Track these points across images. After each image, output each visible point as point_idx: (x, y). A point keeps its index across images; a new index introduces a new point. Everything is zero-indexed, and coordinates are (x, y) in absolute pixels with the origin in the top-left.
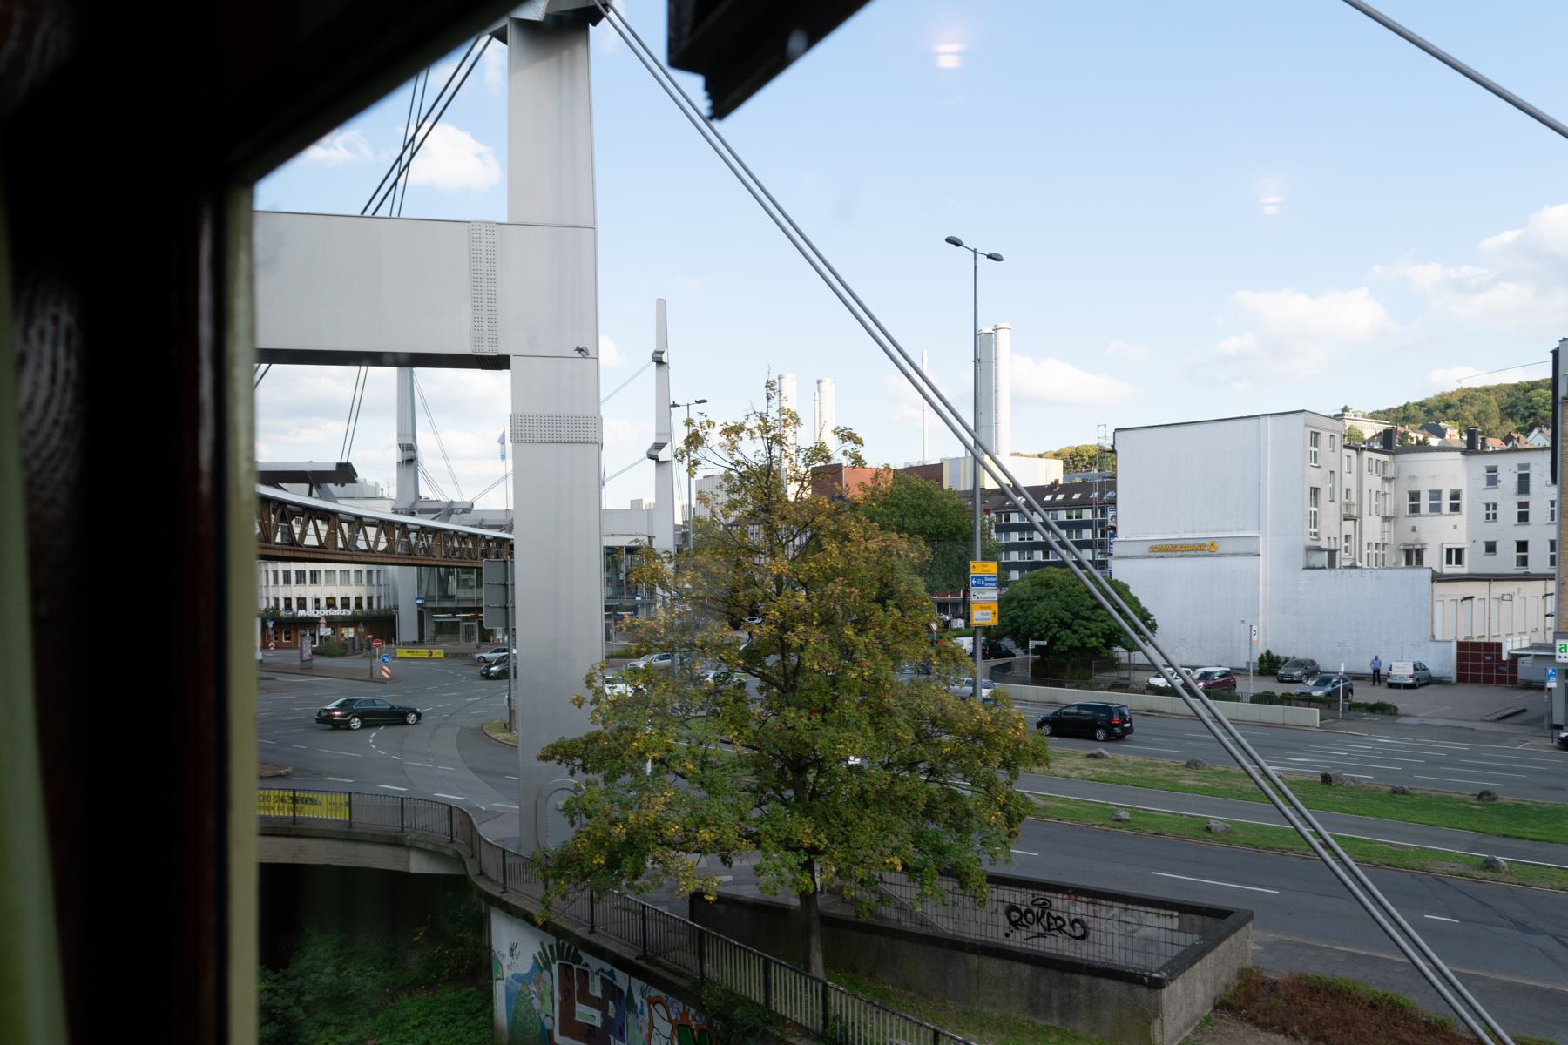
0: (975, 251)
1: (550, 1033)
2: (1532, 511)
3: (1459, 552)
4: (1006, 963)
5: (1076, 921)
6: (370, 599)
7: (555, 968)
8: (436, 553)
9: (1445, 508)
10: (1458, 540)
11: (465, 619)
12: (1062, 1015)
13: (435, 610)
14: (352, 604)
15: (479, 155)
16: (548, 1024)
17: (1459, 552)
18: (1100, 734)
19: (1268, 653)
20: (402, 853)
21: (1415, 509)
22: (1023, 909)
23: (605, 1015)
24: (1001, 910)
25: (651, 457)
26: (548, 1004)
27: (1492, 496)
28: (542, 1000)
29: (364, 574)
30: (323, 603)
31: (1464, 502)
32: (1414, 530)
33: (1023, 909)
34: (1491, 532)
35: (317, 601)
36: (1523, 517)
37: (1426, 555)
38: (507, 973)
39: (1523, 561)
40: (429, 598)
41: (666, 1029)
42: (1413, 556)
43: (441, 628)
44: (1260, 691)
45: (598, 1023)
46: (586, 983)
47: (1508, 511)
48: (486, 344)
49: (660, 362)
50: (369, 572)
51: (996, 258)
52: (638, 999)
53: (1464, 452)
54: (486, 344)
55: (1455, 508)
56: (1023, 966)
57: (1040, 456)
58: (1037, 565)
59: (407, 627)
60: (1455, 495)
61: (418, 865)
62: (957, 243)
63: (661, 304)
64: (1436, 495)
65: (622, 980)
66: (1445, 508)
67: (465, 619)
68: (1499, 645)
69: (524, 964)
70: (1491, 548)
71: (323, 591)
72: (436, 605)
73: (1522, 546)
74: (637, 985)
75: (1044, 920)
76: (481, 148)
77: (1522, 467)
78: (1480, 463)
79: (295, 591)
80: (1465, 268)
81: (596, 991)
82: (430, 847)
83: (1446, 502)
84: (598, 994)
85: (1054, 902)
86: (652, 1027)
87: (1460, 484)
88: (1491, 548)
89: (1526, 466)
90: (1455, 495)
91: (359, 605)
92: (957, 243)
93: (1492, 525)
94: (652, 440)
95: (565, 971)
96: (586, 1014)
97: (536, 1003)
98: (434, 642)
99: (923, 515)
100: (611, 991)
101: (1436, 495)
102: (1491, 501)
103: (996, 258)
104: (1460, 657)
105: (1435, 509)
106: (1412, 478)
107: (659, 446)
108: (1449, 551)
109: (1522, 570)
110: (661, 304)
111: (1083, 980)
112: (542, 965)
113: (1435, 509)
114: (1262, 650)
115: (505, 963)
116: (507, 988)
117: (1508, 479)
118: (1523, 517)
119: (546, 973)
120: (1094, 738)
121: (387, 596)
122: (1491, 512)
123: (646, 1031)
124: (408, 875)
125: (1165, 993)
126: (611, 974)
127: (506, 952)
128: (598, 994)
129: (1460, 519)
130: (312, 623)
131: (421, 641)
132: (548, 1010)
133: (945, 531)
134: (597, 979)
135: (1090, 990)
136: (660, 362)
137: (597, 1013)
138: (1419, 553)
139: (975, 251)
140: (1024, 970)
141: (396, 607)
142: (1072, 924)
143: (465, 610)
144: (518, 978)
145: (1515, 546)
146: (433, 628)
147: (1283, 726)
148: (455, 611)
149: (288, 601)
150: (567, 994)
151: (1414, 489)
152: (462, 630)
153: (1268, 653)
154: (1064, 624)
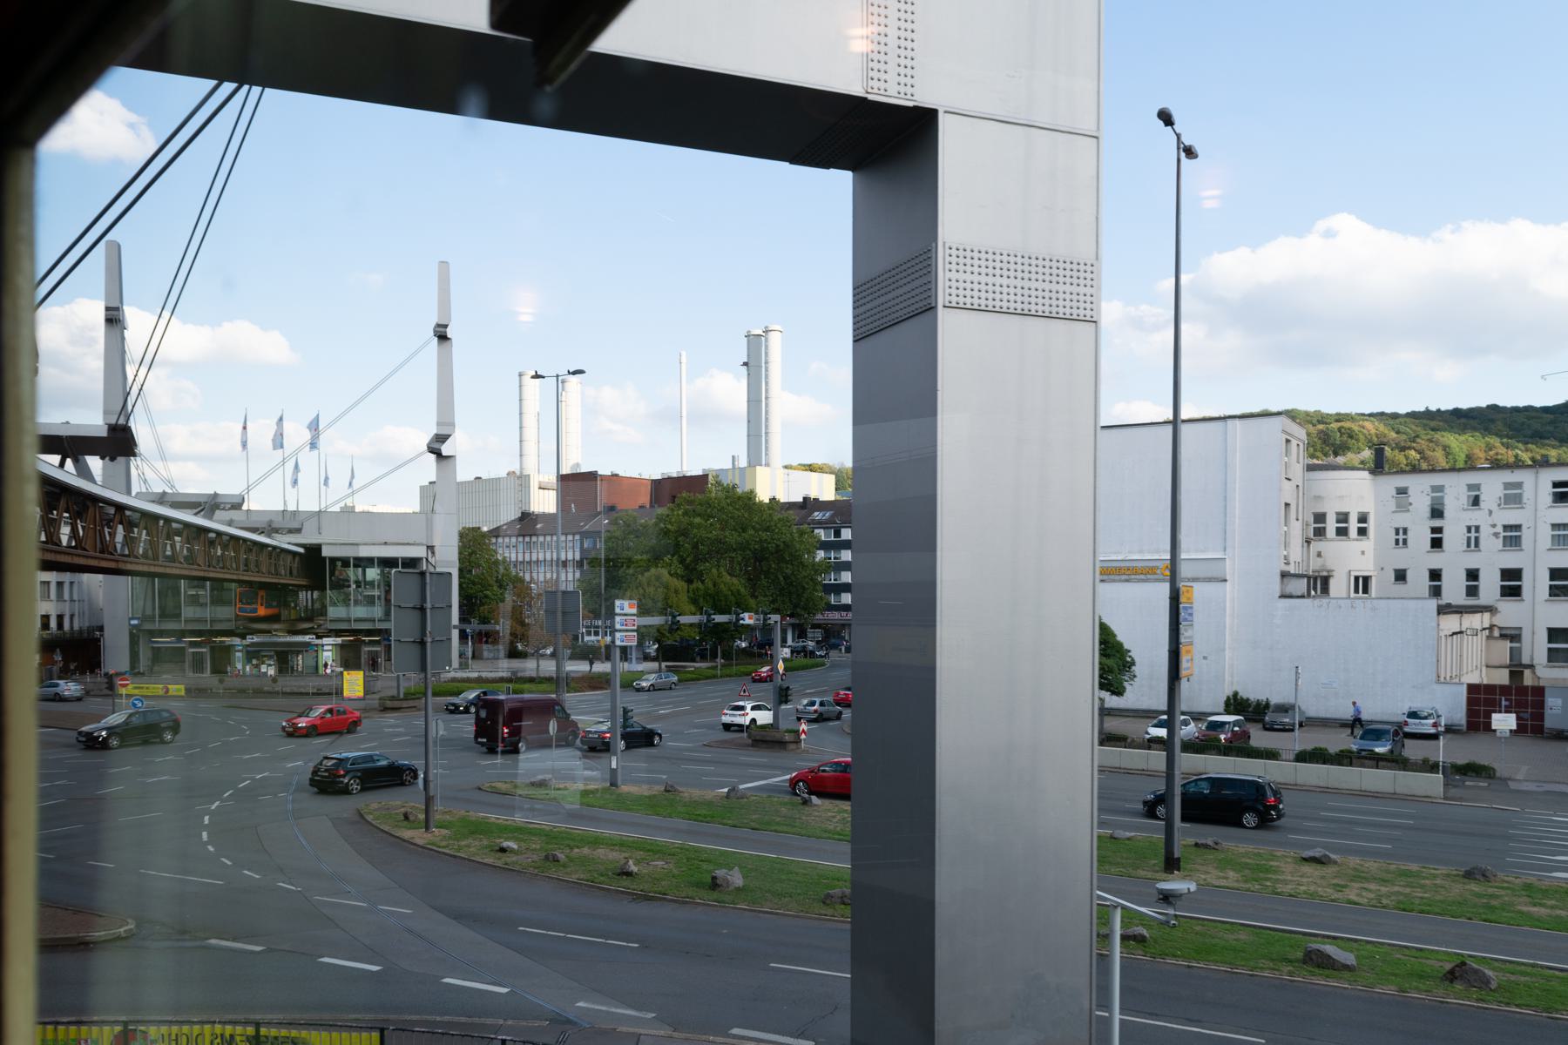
2: (1447, 537)
3: (1366, 579)
6: (60, 618)
8: (200, 561)
9: (1353, 532)
10: (1366, 567)
11: (193, 644)
13: (152, 633)
14: (53, 624)
15: (131, 126)
17: (1366, 579)
18: (1250, 819)
19: (1236, 694)
21: (1320, 532)
25: (432, 450)
27: (1402, 520)
29: (53, 588)
31: (1371, 525)
32: (1319, 555)
34: (1401, 559)
36: (1437, 544)
37: (1332, 582)
39: (1472, 591)
40: (144, 618)
42: (1320, 583)
43: (158, 655)
44: (1309, 747)
47: (1420, 535)
48: (892, 77)
49: (443, 337)
50: (60, 584)
53: (1372, 472)
54: (892, 77)
55: (1362, 532)
57: (811, 468)
59: (116, 657)
60: (1363, 518)
63: (444, 266)
64: (1343, 517)
66: (1353, 532)
67: (193, 644)
68: (1472, 688)
70: (1401, 576)
72: (156, 626)
73: (1435, 575)
76: (133, 117)
77: (1471, 487)
78: (1391, 483)
80: (1144, 307)
83: (1353, 525)
87: (1368, 507)
88: (1401, 576)
89: (1440, 489)
90: (1363, 518)
91: (60, 625)
93: (1401, 552)
94: (434, 431)
99: (744, 530)
101: (1343, 517)
102: (1401, 525)
104: (1471, 702)
105: (1342, 532)
106: (1318, 498)
107: (441, 438)
108: (1357, 578)
109: (1471, 602)
110: (444, 266)
113: (1342, 532)
114: (1228, 692)
117: (1421, 503)
118: (1437, 544)
120: (1239, 824)
121: (82, 614)
122: (1401, 537)
129: (1367, 545)
133: (772, 547)
136: (443, 337)
138: (1325, 581)
141: (101, 629)
145: (1498, 575)
146: (149, 654)
147: (1393, 797)
148: (182, 634)
151: (1320, 510)
152: (188, 659)
153: (1236, 694)
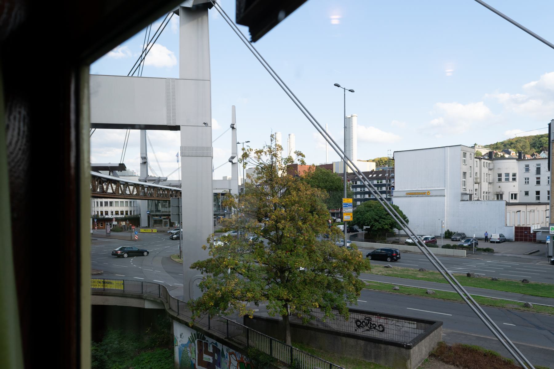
0: (344, 89)
1: (194, 365)
2: (541, 180)
3: (516, 195)
4: (355, 340)
5: (380, 325)
6: (131, 211)
7: (196, 342)
8: (154, 195)
9: (511, 179)
10: (515, 191)
11: (164, 219)
12: (375, 359)
13: (154, 215)
14: (125, 213)
15: (169, 55)
16: (194, 361)
17: (516, 195)
18: (389, 259)
19: (448, 230)
20: (142, 301)
21: (500, 180)
22: (362, 321)
23: (214, 359)
24: (354, 321)
25: (230, 161)
26: (194, 355)
27: (527, 175)
28: (192, 353)
29: (129, 203)
30: (114, 213)
31: (517, 177)
32: (499, 187)
33: (362, 321)
34: (527, 188)
35: (112, 212)
36: (538, 183)
37: (504, 196)
38: (179, 344)
39: (538, 198)
40: (151, 211)
41: (235, 363)
42: (499, 196)
43: (156, 222)
44: (445, 244)
45: (211, 361)
46: (207, 347)
47: (533, 180)
48: (172, 122)
49: (233, 128)
50: (131, 202)
51: (352, 91)
52: (225, 353)
53: (517, 160)
54: (172, 122)
55: (514, 179)
56: (361, 341)
57: (368, 161)
58: (367, 199)
59: (144, 221)
60: (514, 175)
61: (148, 305)
62: (338, 86)
63: (234, 108)
64: (507, 175)
65: (220, 346)
66: (511, 179)
67: (164, 219)
68: (530, 228)
69: (185, 341)
70: (527, 193)
71: (114, 209)
72: (154, 214)
73: (538, 193)
74: (225, 348)
75: (369, 325)
76: (170, 52)
77: (538, 165)
78: (523, 164)
79: (104, 209)
80: (517, 95)
81: (211, 350)
82: (152, 299)
83: (511, 177)
84: (211, 351)
85: (372, 318)
86: (230, 363)
87: (516, 171)
88: (527, 193)
89: (539, 165)
90: (514, 175)
91: (127, 214)
92: (338, 86)
93: (527, 185)
94: (231, 155)
95: (200, 343)
96: (207, 358)
97: (189, 354)
98: (153, 227)
99: (326, 182)
100: (216, 350)
101: (507, 175)
102: (527, 177)
103: (352, 91)
104: (516, 232)
105: (507, 180)
106: (499, 169)
107: (233, 158)
108: (512, 195)
109: (538, 201)
110: (234, 108)
111: (383, 346)
112: (192, 341)
113: (507, 180)
114: (446, 230)
115: (178, 340)
116: (179, 349)
117: (533, 169)
118: (538, 183)
119: (193, 343)
120: (387, 261)
121: (137, 210)
122: (527, 181)
123: (228, 364)
124: (144, 309)
125: (412, 351)
126: (216, 344)
127: (179, 336)
128: (211, 351)
129: (516, 183)
130: (110, 220)
131: (149, 226)
132: (194, 357)
133: (334, 187)
134: (211, 346)
135: (385, 350)
136: (233, 128)
137: (211, 358)
138: (501, 195)
139: (344, 89)
140: (362, 343)
141: (140, 214)
142: (379, 326)
143: (164, 215)
144: (183, 345)
145: (535, 193)
146: (153, 222)
147: (453, 256)
148: (161, 216)
149: (102, 212)
150: (200, 351)
151: (500, 173)
152: (163, 223)
153: (448, 230)
154: (376, 220)
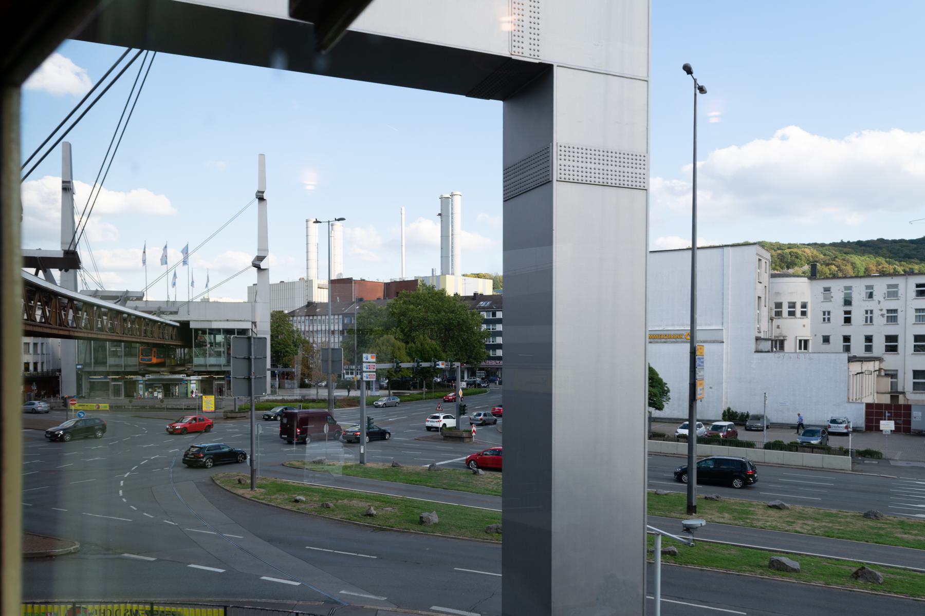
2: (853, 316)
3: (806, 342)
6: (35, 364)
8: (118, 330)
9: (798, 314)
10: (806, 334)
11: (114, 380)
13: (90, 373)
14: (31, 368)
15: (77, 74)
17: (806, 342)
18: (737, 483)
19: (729, 409)
21: (779, 314)
25: (255, 265)
27: (827, 307)
29: (31, 346)
31: (809, 310)
32: (778, 327)
34: (826, 329)
36: (848, 320)
37: (786, 343)
39: (869, 349)
40: (85, 365)
42: (779, 344)
43: (93, 386)
44: (772, 440)
47: (838, 315)
48: (526, 45)
49: (261, 199)
50: (35, 344)
53: (810, 278)
54: (526, 45)
55: (804, 314)
57: (478, 276)
59: (68, 387)
60: (804, 306)
63: (262, 157)
64: (792, 305)
66: (798, 314)
67: (114, 380)
68: (868, 406)
70: (826, 339)
72: (92, 369)
73: (847, 339)
76: (78, 69)
77: (868, 287)
78: (821, 285)
80: (675, 181)
83: (798, 310)
87: (807, 299)
88: (826, 339)
89: (849, 288)
90: (804, 306)
91: (35, 369)
93: (827, 325)
94: (256, 254)
99: (439, 313)
101: (792, 305)
102: (826, 309)
104: (868, 414)
105: (792, 314)
106: (777, 294)
107: (260, 258)
108: (800, 341)
109: (868, 355)
110: (262, 157)
113: (792, 314)
114: (725, 408)
117: (838, 296)
118: (848, 320)
120: (731, 486)
121: (48, 362)
122: (826, 316)
129: (807, 321)
133: (455, 323)
136: (261, 199)
138: (782, 343)
141: (60, 371)
145: (884, 339)
146: (88, 385)
147: (822, 470)
148: (107, 374)
151: (779, 301)
152: (111, 388)
153: (729, 409)
